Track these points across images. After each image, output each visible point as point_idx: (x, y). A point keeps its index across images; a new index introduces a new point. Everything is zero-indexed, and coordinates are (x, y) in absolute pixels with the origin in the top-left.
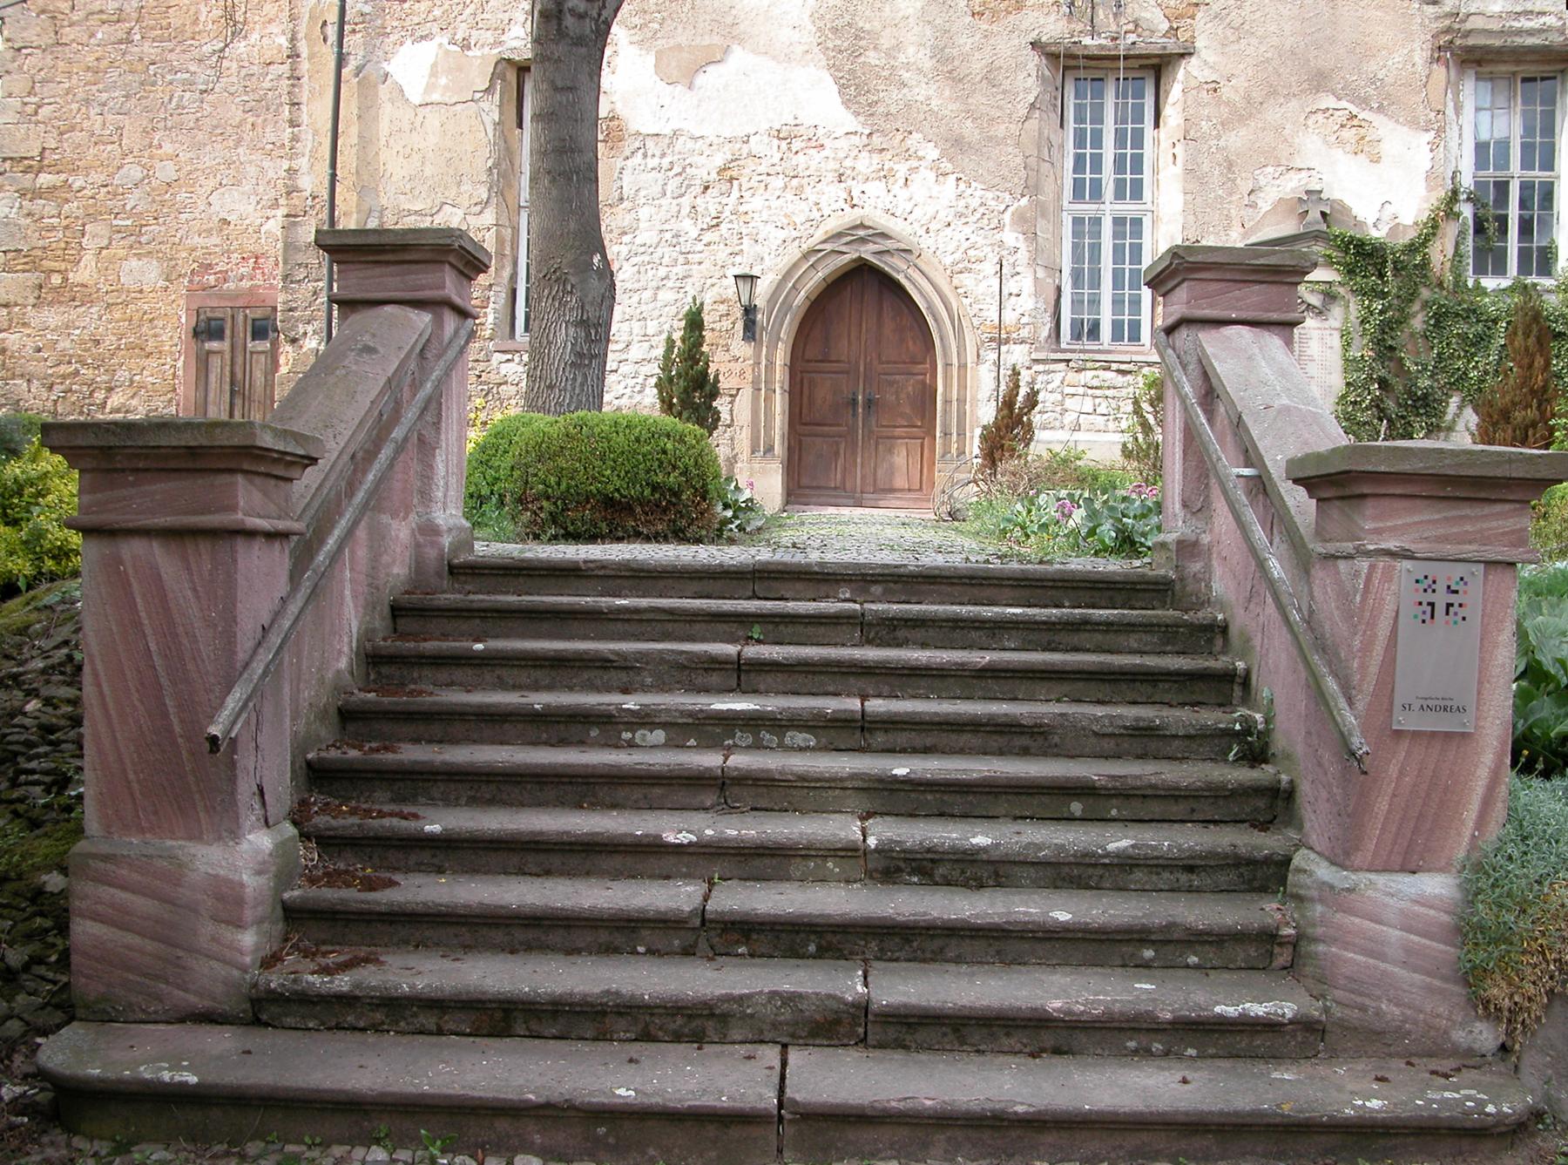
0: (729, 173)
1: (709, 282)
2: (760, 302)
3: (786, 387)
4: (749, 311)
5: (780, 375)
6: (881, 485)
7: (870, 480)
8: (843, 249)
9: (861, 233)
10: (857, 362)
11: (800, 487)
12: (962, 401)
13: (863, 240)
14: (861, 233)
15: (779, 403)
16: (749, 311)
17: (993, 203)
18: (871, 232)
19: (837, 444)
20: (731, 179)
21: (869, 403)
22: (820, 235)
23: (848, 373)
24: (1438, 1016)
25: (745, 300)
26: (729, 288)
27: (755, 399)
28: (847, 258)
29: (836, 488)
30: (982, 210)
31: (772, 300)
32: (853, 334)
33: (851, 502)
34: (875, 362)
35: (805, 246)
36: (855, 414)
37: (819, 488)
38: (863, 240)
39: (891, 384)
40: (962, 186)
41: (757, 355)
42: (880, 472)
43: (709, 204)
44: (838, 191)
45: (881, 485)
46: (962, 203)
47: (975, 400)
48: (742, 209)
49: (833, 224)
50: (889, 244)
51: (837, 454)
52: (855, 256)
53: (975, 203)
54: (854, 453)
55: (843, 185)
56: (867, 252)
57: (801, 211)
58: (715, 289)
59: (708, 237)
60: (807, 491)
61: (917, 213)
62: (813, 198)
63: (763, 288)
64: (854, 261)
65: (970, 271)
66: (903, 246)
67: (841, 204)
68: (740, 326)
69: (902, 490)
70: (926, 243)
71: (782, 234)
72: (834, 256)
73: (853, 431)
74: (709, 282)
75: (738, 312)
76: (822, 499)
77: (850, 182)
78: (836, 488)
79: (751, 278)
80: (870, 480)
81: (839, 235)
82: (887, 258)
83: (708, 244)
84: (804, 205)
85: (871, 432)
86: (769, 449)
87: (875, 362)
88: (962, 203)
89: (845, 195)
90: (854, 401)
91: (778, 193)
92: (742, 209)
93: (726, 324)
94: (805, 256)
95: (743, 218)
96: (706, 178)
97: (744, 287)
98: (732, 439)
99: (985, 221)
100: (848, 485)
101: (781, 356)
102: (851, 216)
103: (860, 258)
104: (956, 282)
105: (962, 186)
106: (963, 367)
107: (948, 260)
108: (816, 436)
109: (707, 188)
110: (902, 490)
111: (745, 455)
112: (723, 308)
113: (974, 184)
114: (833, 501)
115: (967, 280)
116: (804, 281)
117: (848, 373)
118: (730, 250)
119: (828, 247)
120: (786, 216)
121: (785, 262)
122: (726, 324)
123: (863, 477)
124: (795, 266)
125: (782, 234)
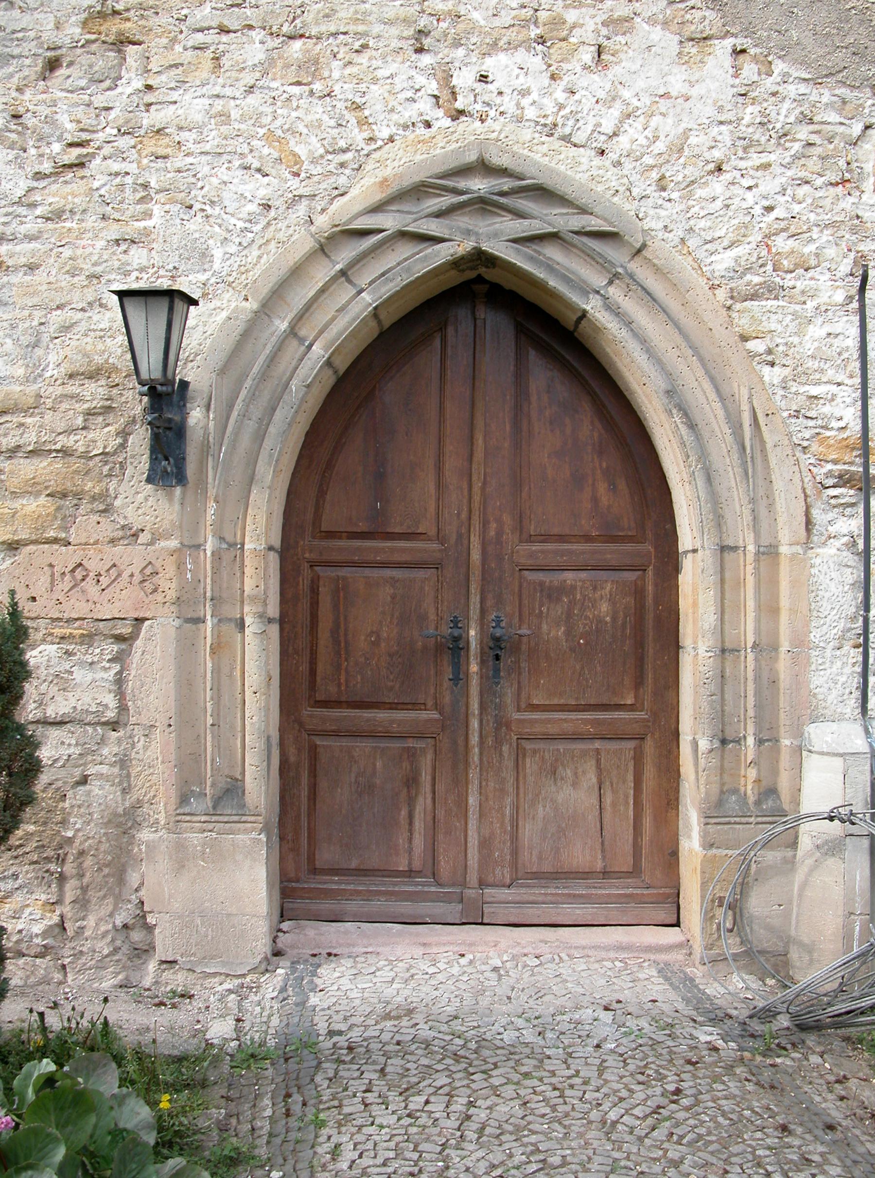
0: (113, 27)
1: (57, 318)
2: (194, 372)
3: (273, 610)
4: (165, 398)
5: (258, 579)
6: (530, 860)
7: (502, 850)
8: (432, 227)
9: (479, 185)
10: (463, 539)
11: (314, 871)
12: (766, 648)
13: (484, 205)
14: (479, 185)
15: (256, 658)
16: (165, 398)
17: (833, 117)
18: (506, 184)
19: (412, 755)
20: (122, 42)
21: (496, 649)
22: (363, 190)
23: (437, 566)
24: (393, 597)
25: (151, 366)
26: (104, 332)
27: (186, 648)
28: (443, 253)
29: (410, 873)
30: (803, 133)
31: (231, 364)
32: (452, 463)
33: (453, 910)
34: (510, 537)
35: (322, 222)
36: (459, 677)
37: (362, 872)
38: (484, 205)
39: (553, 594)
40: (750, 71)
41: (191, 525)
42: (529, 831)
43: (62, 106)
44: (414, 76)
45: (530, 860)
46: (750, 113)
47: (801, 643)
48: (147, 120)
49: (401, 163)
50: (548, 218)
51: (412, 781)
52: (462, 247)
53: (784, 114)
54: (460, 782)
55: (426, 60)
56: (496, 236)
57: (311, 126)
58: (74, 340)
59: (54, 195)
60: (334, 883)
61: (633, 135)
62: (345, 91)
63: (205, 331)
64: (457, 264)
65: (771, 291)
66: (595, 224)
67: (425, 106)
68: (140, 440)
69: (585, 875)
70: (658, 220)
71: (260, 188)
72: (405, 250)
73: (454, 721)
74: (57, 318)
75: (135, 403)
76: (377, 905)
77: (445, 52)
78: (410, 873)
79: (174, 300)
80: (502, 850)
81: (419, 191)
82: (553, 252)
83: (56, 216)
84: (319, 110)
85: (502, 724)
86: (232, 791)
87: (510, 537)
88: (750, 113)
89: (433, 87)
90: (456, 647)
91: (248, 79)
92: (147, 120)
93: (103, 436)
94: (324, 248)
95: (150, 146)
96: (49, 36)
97: (149, 325)
98: (123, 762)
99: (814, 164)
100: (445, 867)
101: (259, 526)
102: (451, 141)
103: (480, 257)
104: (743, 323)
105: (750, 71)
106: (769, 553)
107: (723, 262)
108: (355, 734)
109: (53, 65)
110: (585, 875)
111: (161, 810)
112: (94, 392)
113: (779, 67)
114: (406, 908)
115: (771, 318)
116: (320, 317)
117: (437, 566)
118: (113, 231)
119: (389, 222)
120: (270, 137)
121: (265, 263)
122: (103, 436)
123: (485, 844)
124: (296, 272)
125: (260, 188)
